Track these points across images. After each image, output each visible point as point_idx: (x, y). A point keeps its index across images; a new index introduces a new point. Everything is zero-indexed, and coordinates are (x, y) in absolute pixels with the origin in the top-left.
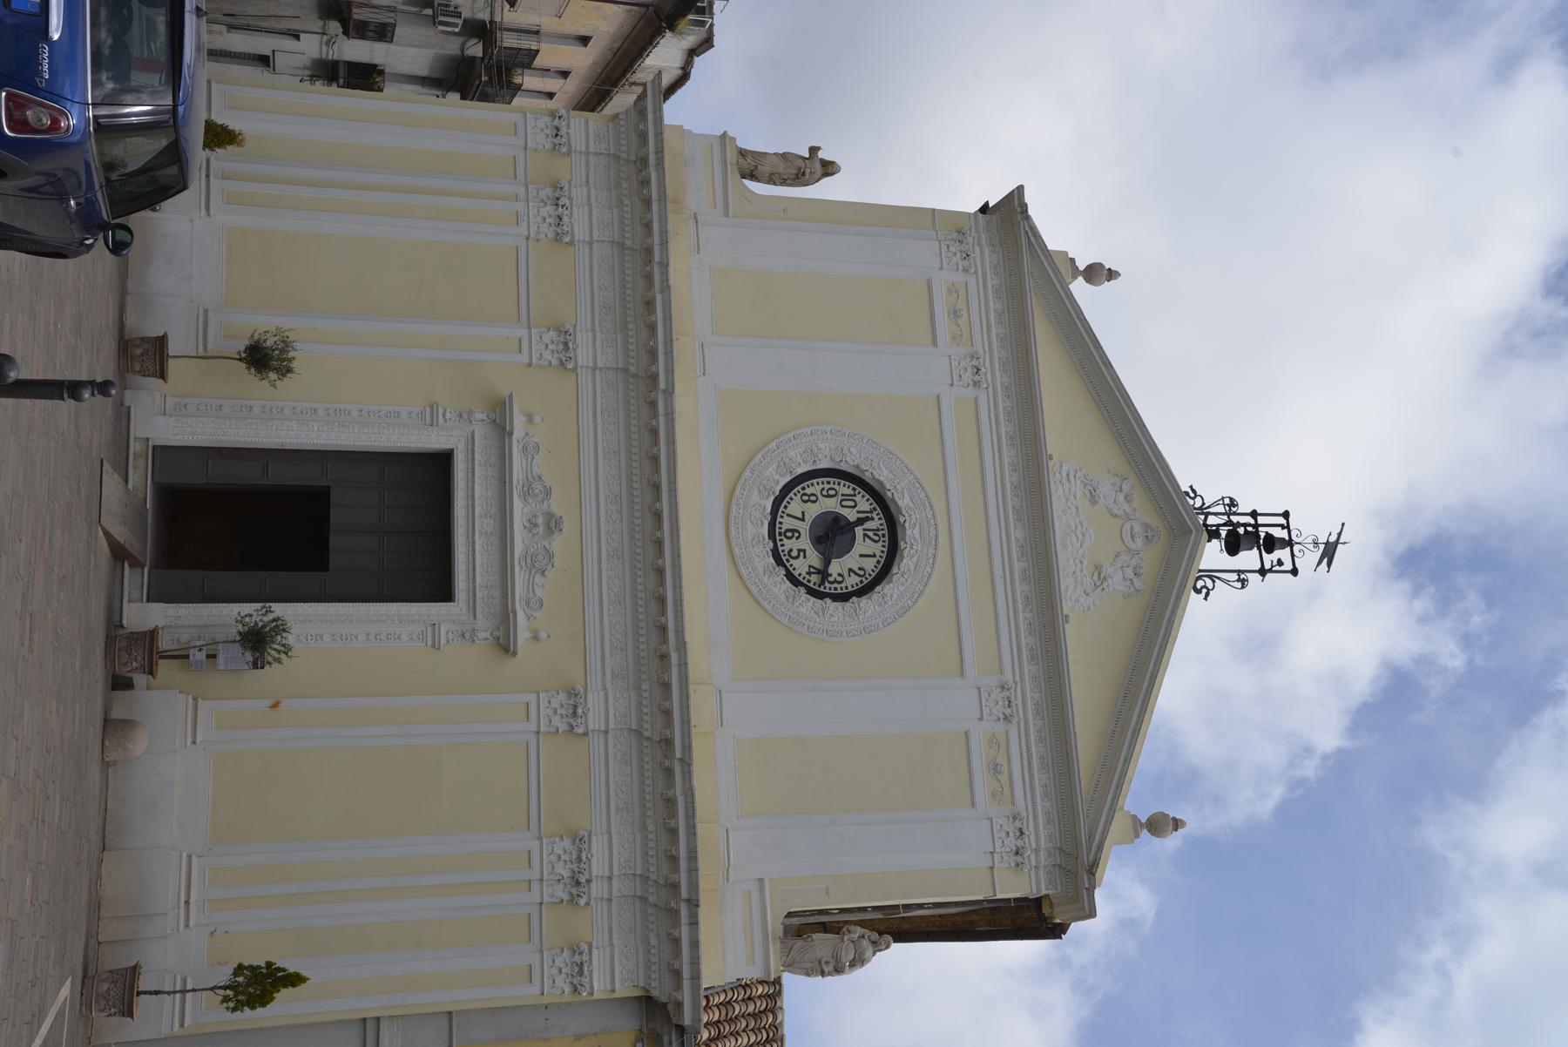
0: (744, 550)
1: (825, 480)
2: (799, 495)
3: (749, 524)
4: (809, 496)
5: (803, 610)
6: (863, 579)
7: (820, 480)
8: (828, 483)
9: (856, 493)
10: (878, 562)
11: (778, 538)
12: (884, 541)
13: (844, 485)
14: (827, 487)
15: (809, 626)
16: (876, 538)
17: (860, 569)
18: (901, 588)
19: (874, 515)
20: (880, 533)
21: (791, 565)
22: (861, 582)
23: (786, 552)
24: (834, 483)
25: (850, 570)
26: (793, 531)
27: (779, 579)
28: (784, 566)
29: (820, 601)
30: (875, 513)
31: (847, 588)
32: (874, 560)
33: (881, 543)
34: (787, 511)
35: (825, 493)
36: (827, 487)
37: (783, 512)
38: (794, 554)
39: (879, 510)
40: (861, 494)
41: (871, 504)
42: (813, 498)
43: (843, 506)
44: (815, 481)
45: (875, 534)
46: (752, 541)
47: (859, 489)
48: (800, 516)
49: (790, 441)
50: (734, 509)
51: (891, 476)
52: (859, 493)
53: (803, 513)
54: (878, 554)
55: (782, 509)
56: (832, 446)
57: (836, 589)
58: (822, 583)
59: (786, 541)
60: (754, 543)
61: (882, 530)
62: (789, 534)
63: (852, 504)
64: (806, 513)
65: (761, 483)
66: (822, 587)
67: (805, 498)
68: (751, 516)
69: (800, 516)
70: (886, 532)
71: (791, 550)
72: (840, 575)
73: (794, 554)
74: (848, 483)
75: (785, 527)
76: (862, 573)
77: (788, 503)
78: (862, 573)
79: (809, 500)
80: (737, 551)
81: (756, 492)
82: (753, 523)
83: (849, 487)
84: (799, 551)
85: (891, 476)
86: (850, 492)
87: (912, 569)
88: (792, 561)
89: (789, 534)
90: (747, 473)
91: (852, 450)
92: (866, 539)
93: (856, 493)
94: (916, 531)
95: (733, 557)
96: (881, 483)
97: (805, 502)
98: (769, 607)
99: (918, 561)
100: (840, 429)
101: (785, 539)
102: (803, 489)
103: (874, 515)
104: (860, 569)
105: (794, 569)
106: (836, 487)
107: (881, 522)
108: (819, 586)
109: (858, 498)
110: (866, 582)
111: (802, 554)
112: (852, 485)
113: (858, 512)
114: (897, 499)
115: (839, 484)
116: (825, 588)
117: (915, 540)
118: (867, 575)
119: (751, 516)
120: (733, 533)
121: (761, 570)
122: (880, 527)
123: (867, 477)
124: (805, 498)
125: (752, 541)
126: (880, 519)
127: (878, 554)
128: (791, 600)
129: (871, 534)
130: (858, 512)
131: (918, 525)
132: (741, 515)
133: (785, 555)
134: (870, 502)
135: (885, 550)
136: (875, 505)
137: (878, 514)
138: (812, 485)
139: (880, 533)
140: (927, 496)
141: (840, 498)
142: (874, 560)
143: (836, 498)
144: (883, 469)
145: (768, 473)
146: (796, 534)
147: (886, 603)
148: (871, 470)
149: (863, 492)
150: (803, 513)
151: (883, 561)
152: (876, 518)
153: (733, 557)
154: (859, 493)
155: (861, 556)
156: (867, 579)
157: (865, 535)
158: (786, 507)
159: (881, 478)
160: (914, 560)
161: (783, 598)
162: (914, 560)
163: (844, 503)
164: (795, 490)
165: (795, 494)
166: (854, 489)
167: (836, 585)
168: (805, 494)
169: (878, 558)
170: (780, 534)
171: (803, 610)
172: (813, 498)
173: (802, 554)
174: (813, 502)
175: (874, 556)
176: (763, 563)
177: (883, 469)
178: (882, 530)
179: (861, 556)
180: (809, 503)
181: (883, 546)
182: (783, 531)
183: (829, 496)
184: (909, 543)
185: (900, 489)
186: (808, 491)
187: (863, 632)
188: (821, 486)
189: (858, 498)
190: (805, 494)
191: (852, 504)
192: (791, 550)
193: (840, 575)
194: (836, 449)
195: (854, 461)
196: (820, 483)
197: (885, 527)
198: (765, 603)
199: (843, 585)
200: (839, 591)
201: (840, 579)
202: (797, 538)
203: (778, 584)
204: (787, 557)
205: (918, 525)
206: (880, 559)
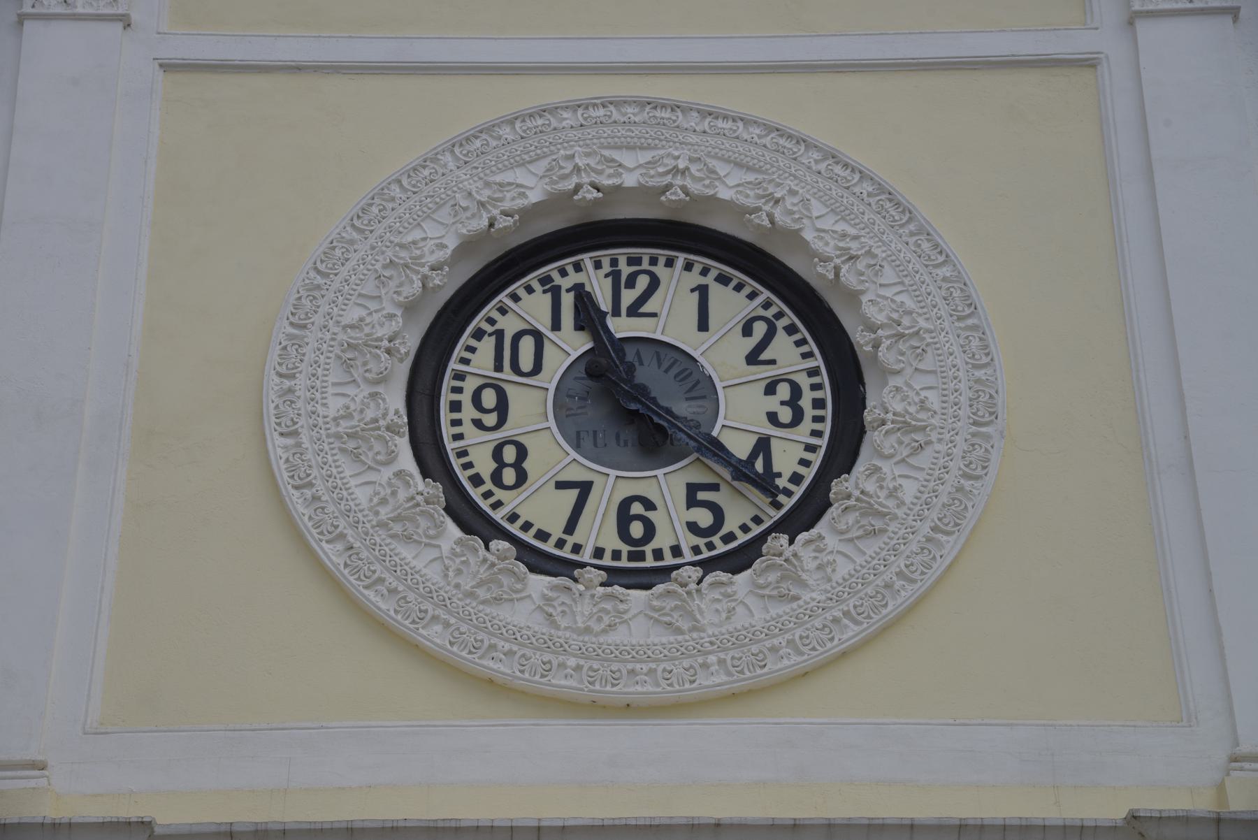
0: (712, 659)
1: (445, 416)
2: (499, 494)
3: (613, 638)
4: (501, 464)
5: (909, 490)
6: (781, 324)
7: (447, 431)
8: (456, 406)
9: (489, 328)
10: (723, 280)
11: (650, 562)
12: (654, 261)
13: (465, 361)
14: (468, 412)
15: (900, 574)
16: (643, 282)
17: (747, 331)
18: (817, 209)
19: (565, 283)
20: (626, 270)
21: (744, 528)
22: (791, 330)
23: (701, 542)
24: (458, 390)
25: (753, 358)
26: (624, 517)
27: (807, 554)
28: (762, 538)
29: (832, 512)
30: (558, 280)
31: (813, 372)
32: (716, 291)
33: (660, 270)
34: (557, 532)
35: (490, 420)
36: (468, 412)
37: (560, 544)
38: (704, 518)
39: (551, 269)
40: (495, 315)
41: (530, 290)
42: (510, 454)
43: (537, 368)
44: (450, 446)
45: (631, 283)
46: (679, 631)
47: (478, 321)
48: (573, 494)
49: (315, 498)
50: (561, 682)
51: (444, 215)
52: (492, 321)
53: (561, 485)
54: (695, 278)
55: (549, 547)
56: (336, 375)
57: (818, 404)
58: (766, 483)
59: (662, 540)
60: (685, 625)
61: (614, 262)
62: (637, 530)
63: (527, 345)
64: (564, 477)
65: (471, 595)
66: (781, 498)
67: (509, 476)
68: (588, 630)
69: (573, 494)
70: (622, 254)
71: (693, 527)
72: (770, 389)
73: (704, 518)
74: (458, 351)
75: (612, 542)
76: (760, 329)
77: (527, 526)
78: (760, 329)
79: (518, 466)
80: (715, 680)
81: (504, 613)
82: (611, 626)
83: (472, 350)
84: (692, 502)
85: (444, 215)
86: (486, 347)
87: (751, 177)
88: (731, 525)
89: (637, 530)
90: (434, 636)
91: (354, 314)
92: (646, 308)
93: (489, 328)
94: (627, 159)
95: (734, 696)
96: (467, 246)
97: (522, 478)
98: (907, 593)
99: (728, 161)
100: (277, 350)
101: (655, 544)
102: (477, 480)
103: (565, 283)
104: (747, 331)
105: (757, 520)
106: (470, 385)
107: (589, 265)
108: (777, 506)
109: (510, 326)
110: (791, 317)
111: (701, 496)
112: (466, 339)
113: (556, 326)
114: (520, 203)
115: (460, 376)
116: (789, 493)
117: (652, 163)
118: (769, 313)
119: (588, 630)
120: (649, 688)
121: (777, 610)
122: (607, 268)
123: (448, 285)
124: (509, 476)
125: (679, 631)
126: (578, 267)
127: (695, 278)
128: (878, 524)
129: (628, 297)
130: (556, 326)
131: (606, 153)
132: (586, 664)
133: (711, 546)
134: (522, 293)
135: (681, 258)
136: (532, 278)
137: (563, 273)
138: (462, 453)
139: (626, 270)
140: (511, 122)
141: (507, 374)
142: (716, 291)
143: (510, 390)
144: (417, 235)
145: (433, 574)
146: (637, 508)
147: (869, 253)
148: (426, 270)
149: (489, 310)
150: (561, 485)
151: (717, 267)
152: (573, 278)
153: (734, 696)
154: (492, 321)
155: (703, 325)
156: (780, 315)
157: (634, 311)
158: (543, 536)
159: (452, 243)
160: (722, 169)
161: (871, 547)
162: (722, 169)
163: (526, 363)
164: (485, 505)
165: (497, 505)
166: (479, 334)
167: (806, 402)
168: (497, 478)
169: (709, 280)
170: (633, 556)
171: (909, 490)
172: (510, 454)
173: (701, 496)
174: (522, 452)
175: (703, 291)
176: (750, 601)
177: (417, 235)
178: (614, 262)
179: (703, 325)
180: (526, 465)
181: (670, 263)
182: (625, 549)
183: (502, 408)
184: (668, 179)
185: (487, 192)
186: (485, 467)
187: (970, 322)
188: (467, 428)
189: (510, 326)
190: (497, 478)
191: (527, 345)
192: (693, 527)
193: (770, 389)
194: (347, 365)
195: (442, 246)
196: (457, 430)
197: (605, 255)
198: (893, 606)
199: (804, 382)
200: (827, 394)
201: (784, 391)
202: (649, 505)
203: (825, 558)
204: (716, 539)
205: (606, 153)
206: (713, 274)
